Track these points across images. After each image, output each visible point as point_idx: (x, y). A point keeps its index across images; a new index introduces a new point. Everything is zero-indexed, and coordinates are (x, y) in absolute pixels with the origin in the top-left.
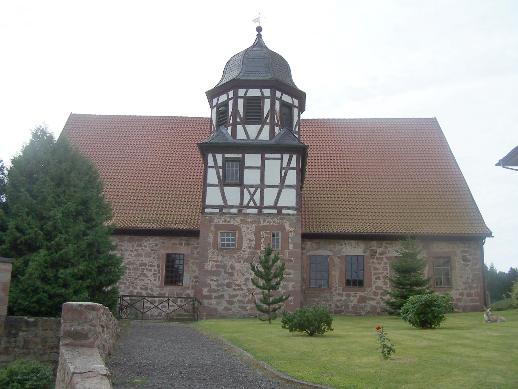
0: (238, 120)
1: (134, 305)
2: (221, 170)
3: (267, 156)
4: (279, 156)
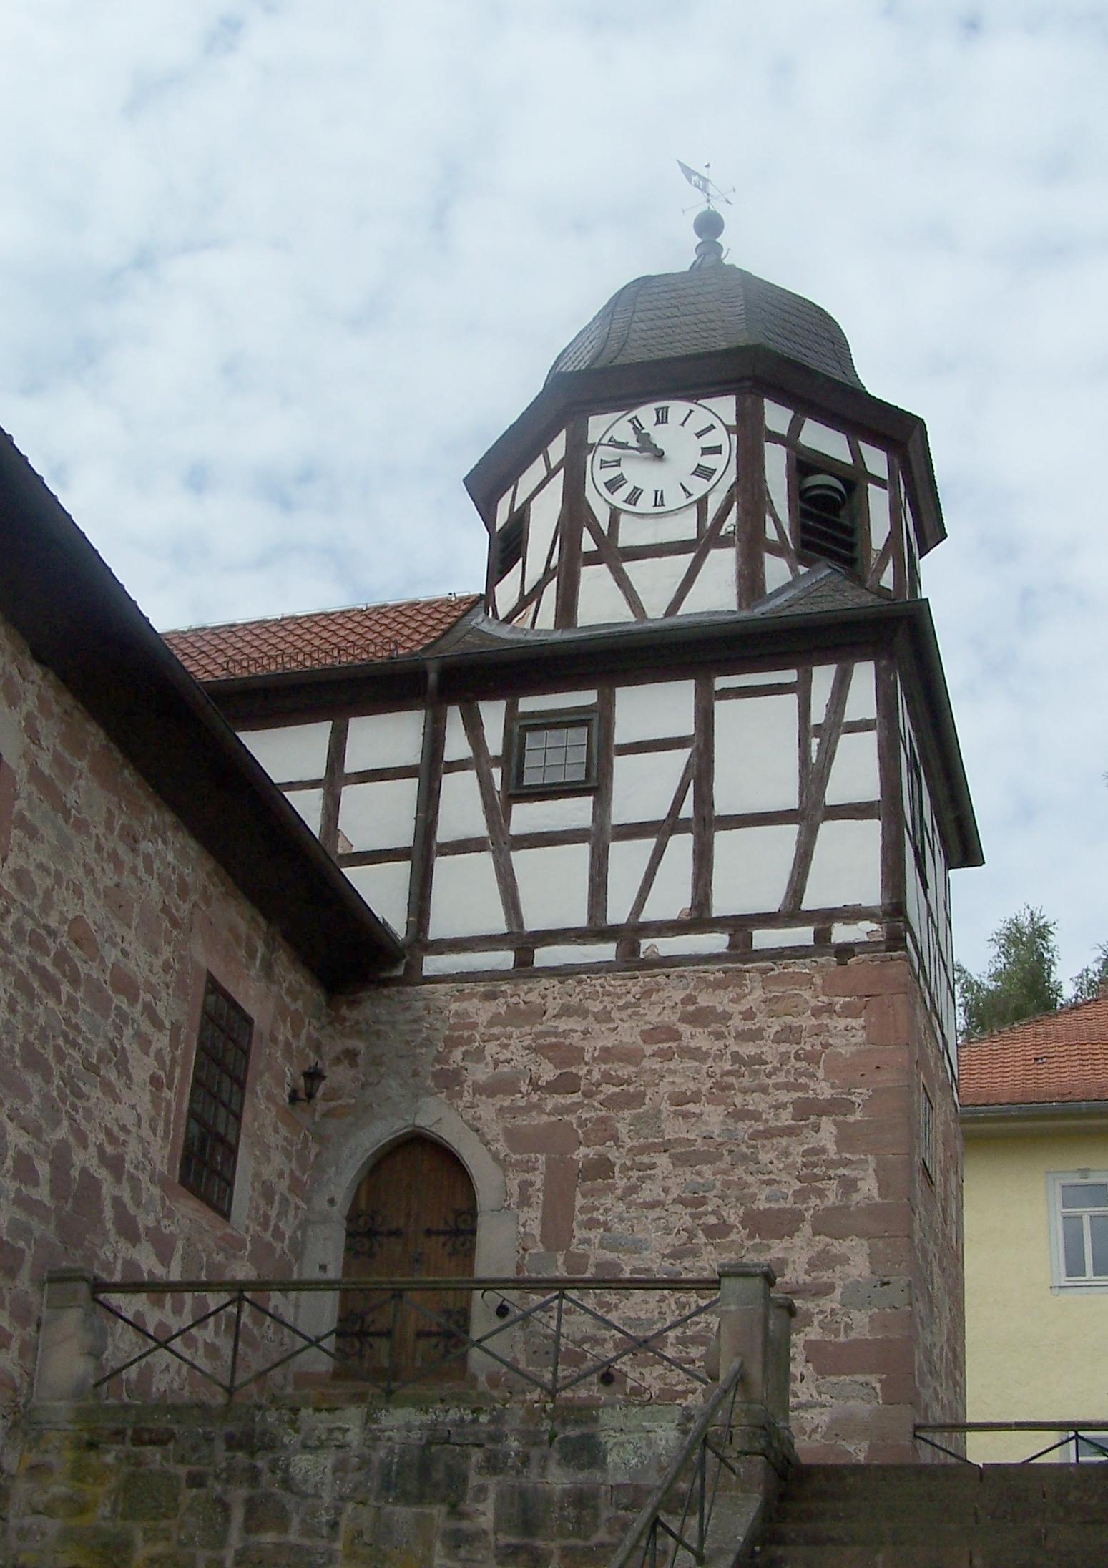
0: (588, 544)
1: (227, 1383)
2: (497, 774)
3: (721, 683)
4: (789, 676)
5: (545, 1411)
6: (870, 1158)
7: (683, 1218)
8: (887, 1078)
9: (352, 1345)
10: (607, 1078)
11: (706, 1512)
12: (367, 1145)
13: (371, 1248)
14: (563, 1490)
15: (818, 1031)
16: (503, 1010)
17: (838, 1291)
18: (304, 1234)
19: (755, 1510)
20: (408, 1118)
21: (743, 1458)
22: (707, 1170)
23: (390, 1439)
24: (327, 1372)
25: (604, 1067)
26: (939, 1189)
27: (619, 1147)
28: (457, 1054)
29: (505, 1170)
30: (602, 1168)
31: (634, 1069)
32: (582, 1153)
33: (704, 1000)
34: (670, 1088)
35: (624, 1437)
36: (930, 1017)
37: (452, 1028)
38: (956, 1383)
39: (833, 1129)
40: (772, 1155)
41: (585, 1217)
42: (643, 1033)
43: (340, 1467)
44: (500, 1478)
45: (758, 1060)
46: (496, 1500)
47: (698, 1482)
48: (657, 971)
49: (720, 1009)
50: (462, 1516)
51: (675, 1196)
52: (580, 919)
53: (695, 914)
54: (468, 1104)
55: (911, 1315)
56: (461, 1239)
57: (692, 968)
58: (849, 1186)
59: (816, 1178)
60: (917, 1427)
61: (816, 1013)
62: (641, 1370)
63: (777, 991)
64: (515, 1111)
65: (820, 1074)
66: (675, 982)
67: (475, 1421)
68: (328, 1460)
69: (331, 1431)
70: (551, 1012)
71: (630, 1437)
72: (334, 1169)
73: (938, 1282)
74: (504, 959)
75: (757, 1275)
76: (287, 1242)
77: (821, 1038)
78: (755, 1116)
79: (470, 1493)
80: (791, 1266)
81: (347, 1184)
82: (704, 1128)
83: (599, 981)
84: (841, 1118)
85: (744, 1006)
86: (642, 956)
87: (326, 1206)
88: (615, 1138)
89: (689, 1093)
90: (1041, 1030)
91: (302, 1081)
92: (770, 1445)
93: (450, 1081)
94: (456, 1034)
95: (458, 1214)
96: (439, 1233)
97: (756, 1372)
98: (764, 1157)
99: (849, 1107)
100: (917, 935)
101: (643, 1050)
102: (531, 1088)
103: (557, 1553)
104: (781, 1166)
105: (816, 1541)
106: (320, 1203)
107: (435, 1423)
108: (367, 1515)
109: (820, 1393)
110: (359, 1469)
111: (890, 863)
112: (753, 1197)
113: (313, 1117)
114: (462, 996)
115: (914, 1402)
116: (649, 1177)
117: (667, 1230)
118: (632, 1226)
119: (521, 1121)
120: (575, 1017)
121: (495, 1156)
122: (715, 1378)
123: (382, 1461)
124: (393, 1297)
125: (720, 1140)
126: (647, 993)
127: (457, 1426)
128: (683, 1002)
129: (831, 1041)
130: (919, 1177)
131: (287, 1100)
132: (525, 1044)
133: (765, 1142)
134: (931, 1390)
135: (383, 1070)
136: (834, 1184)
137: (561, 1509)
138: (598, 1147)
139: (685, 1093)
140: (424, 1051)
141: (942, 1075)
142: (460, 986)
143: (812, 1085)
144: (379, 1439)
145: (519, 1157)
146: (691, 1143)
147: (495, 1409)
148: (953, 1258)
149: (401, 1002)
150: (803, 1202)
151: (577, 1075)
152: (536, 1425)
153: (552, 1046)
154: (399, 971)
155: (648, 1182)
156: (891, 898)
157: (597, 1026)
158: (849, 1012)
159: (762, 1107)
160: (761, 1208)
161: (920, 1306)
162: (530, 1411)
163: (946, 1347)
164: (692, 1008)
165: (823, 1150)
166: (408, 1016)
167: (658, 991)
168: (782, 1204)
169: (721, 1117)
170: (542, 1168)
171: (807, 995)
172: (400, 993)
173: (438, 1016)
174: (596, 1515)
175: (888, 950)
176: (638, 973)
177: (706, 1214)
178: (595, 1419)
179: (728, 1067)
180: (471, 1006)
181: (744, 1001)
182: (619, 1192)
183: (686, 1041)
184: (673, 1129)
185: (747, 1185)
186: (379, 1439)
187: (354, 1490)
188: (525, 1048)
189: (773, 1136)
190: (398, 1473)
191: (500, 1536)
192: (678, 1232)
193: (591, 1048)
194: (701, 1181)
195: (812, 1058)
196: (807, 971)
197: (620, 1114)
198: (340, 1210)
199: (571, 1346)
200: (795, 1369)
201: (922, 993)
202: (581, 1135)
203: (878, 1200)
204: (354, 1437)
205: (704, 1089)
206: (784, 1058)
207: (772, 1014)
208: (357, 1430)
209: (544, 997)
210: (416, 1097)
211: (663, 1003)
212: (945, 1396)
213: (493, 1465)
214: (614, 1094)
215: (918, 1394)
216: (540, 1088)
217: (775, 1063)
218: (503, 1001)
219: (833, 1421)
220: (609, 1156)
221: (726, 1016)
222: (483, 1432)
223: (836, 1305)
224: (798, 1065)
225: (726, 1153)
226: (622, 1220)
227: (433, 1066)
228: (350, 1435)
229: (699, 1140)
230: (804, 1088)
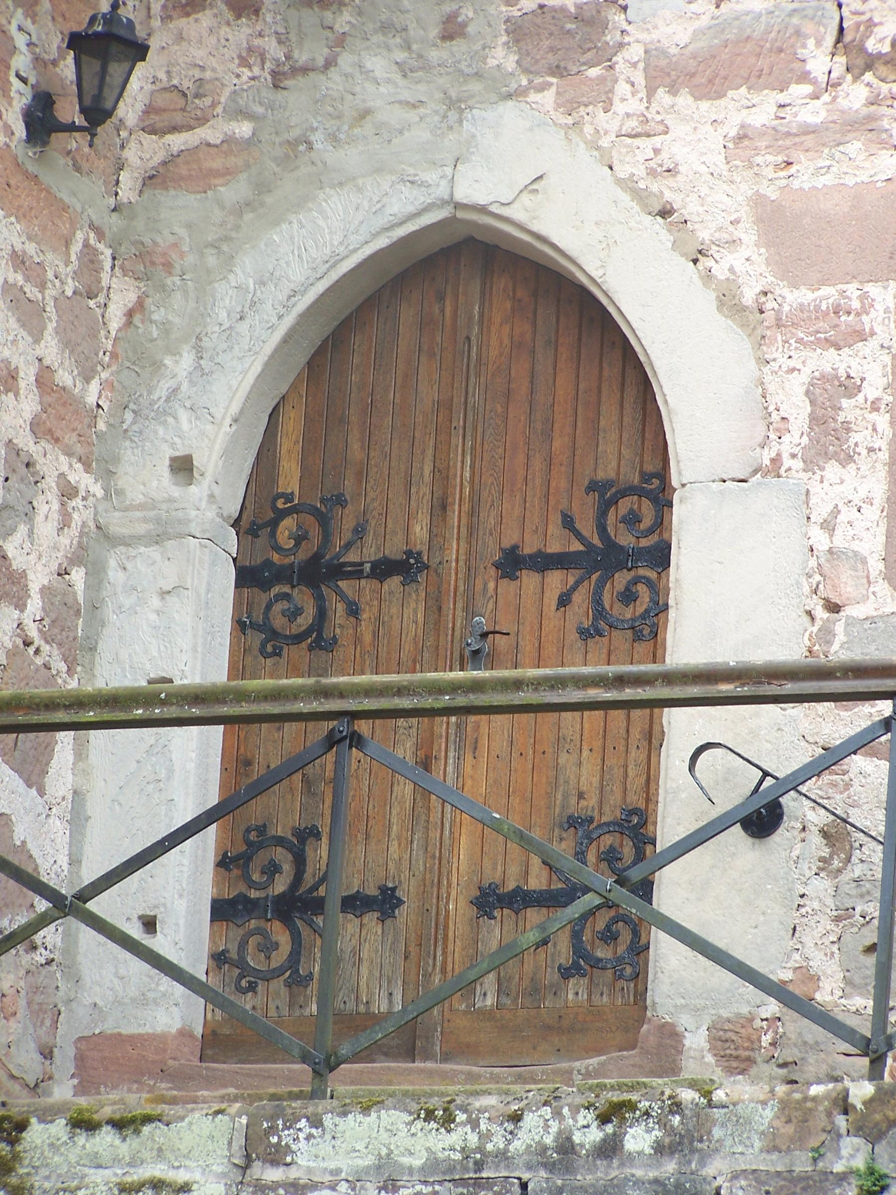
5: (846, 1109)
9: (268, 947)
12: (297, 273)
13: (322, 614)
18: (96, 575)
20: (430, 176)
24: (185, 1033)
54: (632, 124)
56: (621, 579)
72: (187, 360)
76: (35, 605)
81: (235, 408)
91: (67, 68)
102: (841, 60)
124: (332, 741)
127: (550, 1167)
131: (20, 131)
145: (805, 296)
147: (676, 1107)
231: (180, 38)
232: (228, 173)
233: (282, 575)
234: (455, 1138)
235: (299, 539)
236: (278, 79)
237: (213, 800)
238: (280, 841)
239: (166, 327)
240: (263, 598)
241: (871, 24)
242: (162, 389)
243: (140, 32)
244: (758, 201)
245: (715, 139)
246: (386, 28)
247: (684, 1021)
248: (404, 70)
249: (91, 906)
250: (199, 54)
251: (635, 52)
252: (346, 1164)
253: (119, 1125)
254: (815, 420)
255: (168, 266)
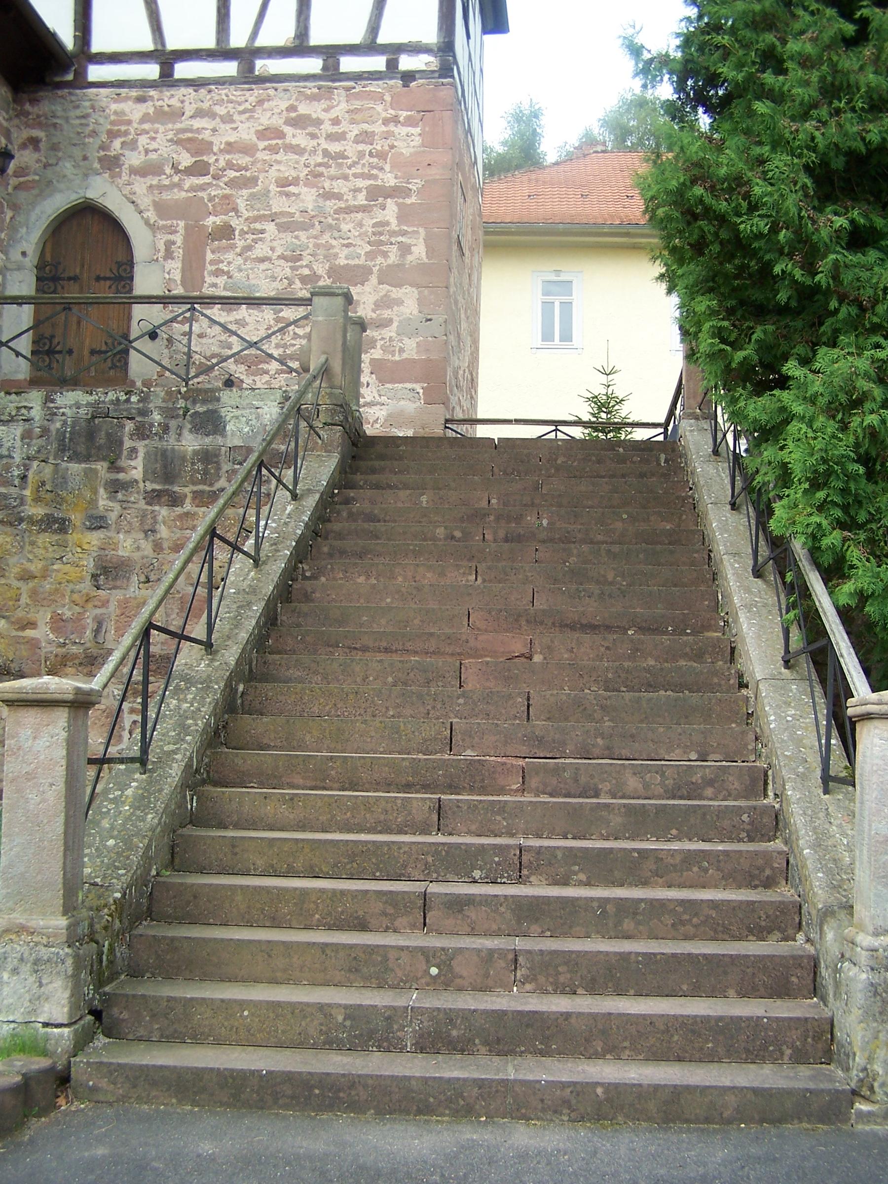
5: (180, 393)
6: (421, 230)
7: (284, 269)
8: (435, 173)
9: (44, 361)
10: (230, 166)
11: (299, 465)
12: (50, 211)
14: (194, 450)
15: (387, 136)
16: (151, 111)
17: (395, 324)
19: (335, 464)
20: (80, 191)
21: (326, 427)
22: (303, 235)
23: (63, 414)
24: (25, 380)
25: (228, 157)
26: (467, 261)
27: (238, 217)
28: (117, 144)
29: (154, 232)
30: (226, 232)
31: (251, 159)
32: (211, 221)
33: (304, 109)
34: (276, 174)
35: (239, 412)
36: (467, 138)
37: (113, 123)
38: (472, 397)
39: (395, 208)
40: (350, 226)
41: (214, 268)
42: (257, 132)
43: (27, 435)
44: (147, 442)
45: (342, 155)
46: (144, 458)
47: (293, 444)
48: (268, 85)
49: (314, 116)
50: (120, 470)
51: (279, 253)
52: (209, 42)
53: (297, 42)
55: (446, 342)
56: (123, 283)
57: (294, 84)
58: (405, 250)
59: (381, 243)
60: (447, 421)
61: (386, 122)
62: (253, 378)
63: (357, 104)
64: (161, 188)
65: (387, 167)
66: (282, 94)
67: (128, 401)
68: (18, 430)
69: (18, 408)
70: (188, 114)
71: (243, 412)
73: (464, 325)
74: (152, 71)
75: (338, 295)
77: (388, 141)
78: (339, 197)
79: (125, 453)
80: (362, 306)
82: (301, 205)
83: (224, 92)
84: (401, 200)
85: (333, 114)
86: (257, 73)
87: (19, 257)
88: (235, 210)
89: (290, 178)
90: (533, 176)
92: (346, 418)
93: (112, 164)
94: (116, 128)
95: (119, 264)
96: (106, 279)
97: (337, 366)
98: (345, 227)
99: (407, 192)
100: (461, 70)
101: (256, 145)
103: (190, 496)
104: (357, 234)
105: (377, 486)
106: (15, 255)
107: (98, 402)
108: (48, 470)
109: (380, 395)
110: (41, 436)
111: (445, 10)
112: (336, 256)
113: (7, 189)
114: (118, 98)
115: (445, 403)
116: (261, 239)
117: (274, 278)
118: (248, 275)
119: (167, 196)
120: (206, 119)
121: (147, 222)
122: (306, 370)
123: (58, 430)
124: (65, 309)
125: (313, 213)
126: (260, 102)
128: (288, 110)
129: (396, 144)
130: (455, 247)
132: (169, 137)
133: (346, 216)
134: (456, 398)
135: (60, 154)
136: (395, 248)
137: (193, 464)
138: (223, 217)
139: (287, 178)
140: (91, 140)
141: (473, 180)
142: (118, 91)
143: (381, 175)
144: (55, 414)
145: (165, 223)
146: (292, 215)
148: (474, 313)
149: (72, 102)
150: (372, 260)
151: (207, 162)
152: (174, 404)
153: (189, 140)
154: (70, 77)
155: (260, 243)
156: (445, 37)
157: (222, 126)
158: (410, 122)
159: (344, 190)
160: (342, 264)
161: (452, 338)
162: (169, 393)
163: (467, 371)
164: (293, 115)
165: (387, 223)
166: (78, 112)
167: (269, 100)
168: (356, 262)
169: (314, 198)
170: (181, 231)
171: (379, 108)
172: (70, 93)
173: (102, 113)
174: (218, 469)
175: (440, 77)
176: (254, 86)
177: (302, 267)
178: (218, 400)
179: (319, 159)
180: (128, 107)
181: (332, 111)
182: (238, 250)
183: (289, 139)
184: (279, 204)
185: (333, 247)
186: (55, 414)
187: (39, 451)
188: (169, 141)
189: (352, 212)
190: (71, 440)
191: (148, 484)
192: (281, 280)
193: (218, 143)
194: (298, 243)
195: (382, 156)
196: (380, 90)
197: (240, 193)
198: (31, 260)
199: (203, 360)
200: (364, 378)
201: (462, 116)
202: (211, 208)
203: (426, 261)
204: (37, 413)
205: (302, 175)
206: (361, 155)
207: (353, 122)
208: (39, 408)
209: (182, 102)
210: (86, 176)
211: (272, 110)
212: (466, 404)
213: (141, 433)
214: (235, 177)
215: (448, 399)
216: (180, 171)
217: (355, 159)
218: (152, 104)
219: (390, 415)
220: (231, 223)
221: (318, 122)
222: (134, 408)
223: (393, 334)
224: (371, 160)
225: (317, 223)
226: (240, 270)
227: (98, 152)
228: (33, 413)
229: (298, 213)
230: (375, 177)
231: (22, 155)
232: (33, 188)
233: (47, 279)
234: (93, 398)
235: (51, 271)
236: (45, 167)
237: (31, 325)
238: (46, 338)
239: (20, 222)
240: (42, 284)
241: (180, 163)
242: (19, 236)
243: (13, 153)
244: (154, 201)
245: (144, 187)
246: (70, 157)
247: (136, 379)
248: (73, 166)
249: (9, 344)
250: (26, 159)
251: (127, 166)
252: (68, 403)
253: (16, 393)
254: (166, 250)
255: (20, 208)
